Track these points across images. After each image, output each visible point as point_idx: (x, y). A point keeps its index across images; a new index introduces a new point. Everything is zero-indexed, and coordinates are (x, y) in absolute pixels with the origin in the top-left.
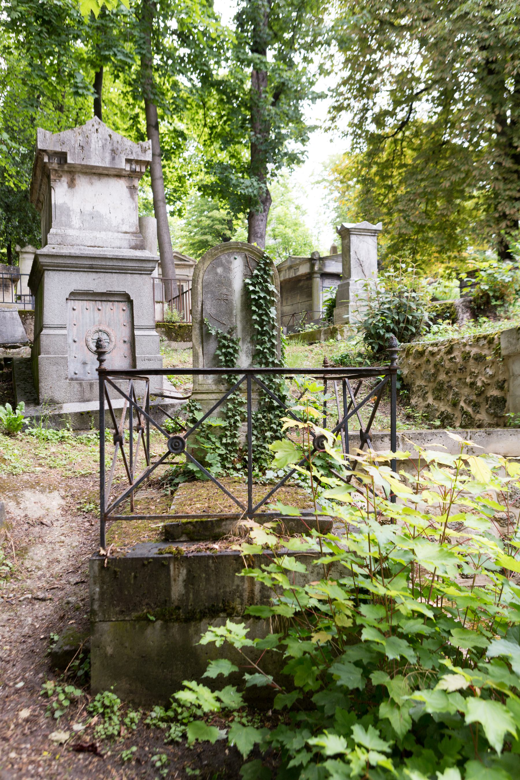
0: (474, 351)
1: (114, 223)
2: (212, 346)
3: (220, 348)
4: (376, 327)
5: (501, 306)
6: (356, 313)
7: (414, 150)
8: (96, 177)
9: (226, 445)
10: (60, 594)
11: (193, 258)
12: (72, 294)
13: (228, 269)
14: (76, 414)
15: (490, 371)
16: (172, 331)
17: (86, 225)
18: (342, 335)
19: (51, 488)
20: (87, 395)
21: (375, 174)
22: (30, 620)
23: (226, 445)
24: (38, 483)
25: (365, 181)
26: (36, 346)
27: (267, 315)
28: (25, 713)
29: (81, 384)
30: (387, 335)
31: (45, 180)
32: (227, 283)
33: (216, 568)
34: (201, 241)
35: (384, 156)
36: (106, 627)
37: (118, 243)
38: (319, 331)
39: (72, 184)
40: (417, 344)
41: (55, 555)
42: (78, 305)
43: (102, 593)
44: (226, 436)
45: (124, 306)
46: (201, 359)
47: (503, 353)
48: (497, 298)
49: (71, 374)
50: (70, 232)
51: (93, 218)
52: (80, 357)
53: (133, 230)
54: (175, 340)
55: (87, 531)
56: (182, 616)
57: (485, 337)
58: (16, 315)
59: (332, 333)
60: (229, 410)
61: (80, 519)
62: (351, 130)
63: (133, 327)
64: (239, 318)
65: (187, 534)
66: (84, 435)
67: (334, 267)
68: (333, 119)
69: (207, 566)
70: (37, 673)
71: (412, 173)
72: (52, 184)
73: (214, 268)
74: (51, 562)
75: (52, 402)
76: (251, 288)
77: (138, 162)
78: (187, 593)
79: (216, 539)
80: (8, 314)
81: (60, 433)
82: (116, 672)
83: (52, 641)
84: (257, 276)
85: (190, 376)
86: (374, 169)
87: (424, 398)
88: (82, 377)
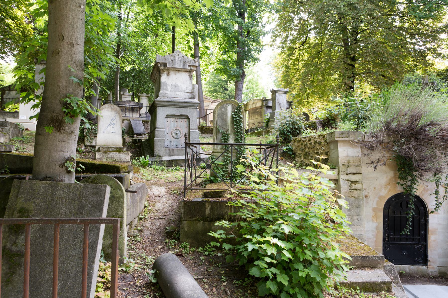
0: (318, 140)
1: (183, 89)
2: (220, 136)
3: (223, 137)
4: (283, 130)
5: (334, 123)
6: (277, 125)
7: (308, 53)
8: (177, 72)
9: (224, 171)
10: (168, 217)
11: (210, 97)
12: (167, 115)
13: (226, 109)
14: (167, 161)
15: (323, 148)
16: (203, 130)
17: (173, 90)
18: (271, 133)
19: (161, 185)
20: (171, 154)
21: (291, 64)
22: (158, 224)
23: (224, 171)
24: (156, 183)
25: (287, 67)
26: (152, 134)
27: (240, 126)
28: (160, 247)
29: (169, 150)
30: (288, 134)
31: (158, 73)
32: (225, 114)
33: (220, 205)
34: (214, 90)
35: (295, 57)
36: (185, 222)
37: (185, 97)
38: (263, 131)
39: (168, 74)
40: (298, 138)
41: (164, 206)
42: (169, 119)
43: (184, 212)
44: (224, 168)
45: (186, 120)
46: (216, 141)
47: (327, 141)
48: (332, 120)
49: (166, 146)
50: (167, 92)
51: (176, 87)
52: (169, 139)
53: (190, 91)
54: (204, 133)
55: (175, 199)
56: (209, 220)
57: (322, 135)
58: (141, 122)
59: (268, 132)
60: (226, 159)
61: (172, 196)
62: (281, 45)
63: (189, 128)
64: (230, 126)
65: (211, 195)
66: (170, 168)
67: (270, 104)
68: (273, 41)
69: (217, 205)
70: (162, 237)
71: (306, 66)
72: (161, 74)
73: (221, 109)
74: (163, 208)
75: (159, 156)
76: (234, 116)
77: (193, 66)
78: (211, 213)
79: (220, 197)
80: (138, 122)
81: (162, 167)
82: (188, 236)
83: (167, 229)
84: (236, 112)
85: (211, 146)
86: (290, 62)
87: (300, 158)
88: (169, 147)
